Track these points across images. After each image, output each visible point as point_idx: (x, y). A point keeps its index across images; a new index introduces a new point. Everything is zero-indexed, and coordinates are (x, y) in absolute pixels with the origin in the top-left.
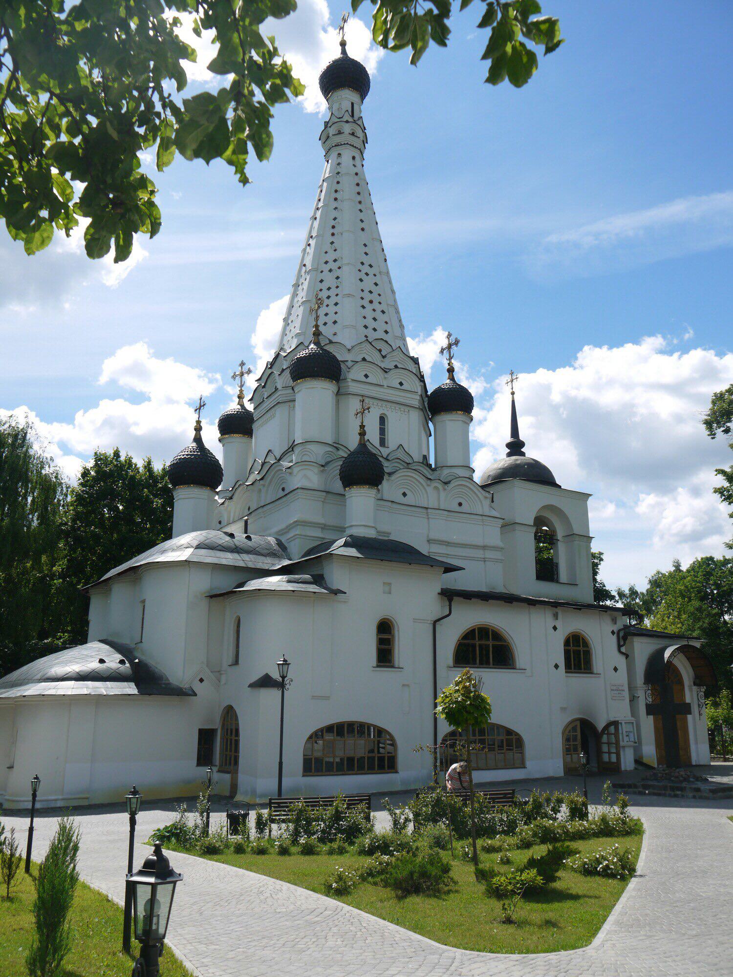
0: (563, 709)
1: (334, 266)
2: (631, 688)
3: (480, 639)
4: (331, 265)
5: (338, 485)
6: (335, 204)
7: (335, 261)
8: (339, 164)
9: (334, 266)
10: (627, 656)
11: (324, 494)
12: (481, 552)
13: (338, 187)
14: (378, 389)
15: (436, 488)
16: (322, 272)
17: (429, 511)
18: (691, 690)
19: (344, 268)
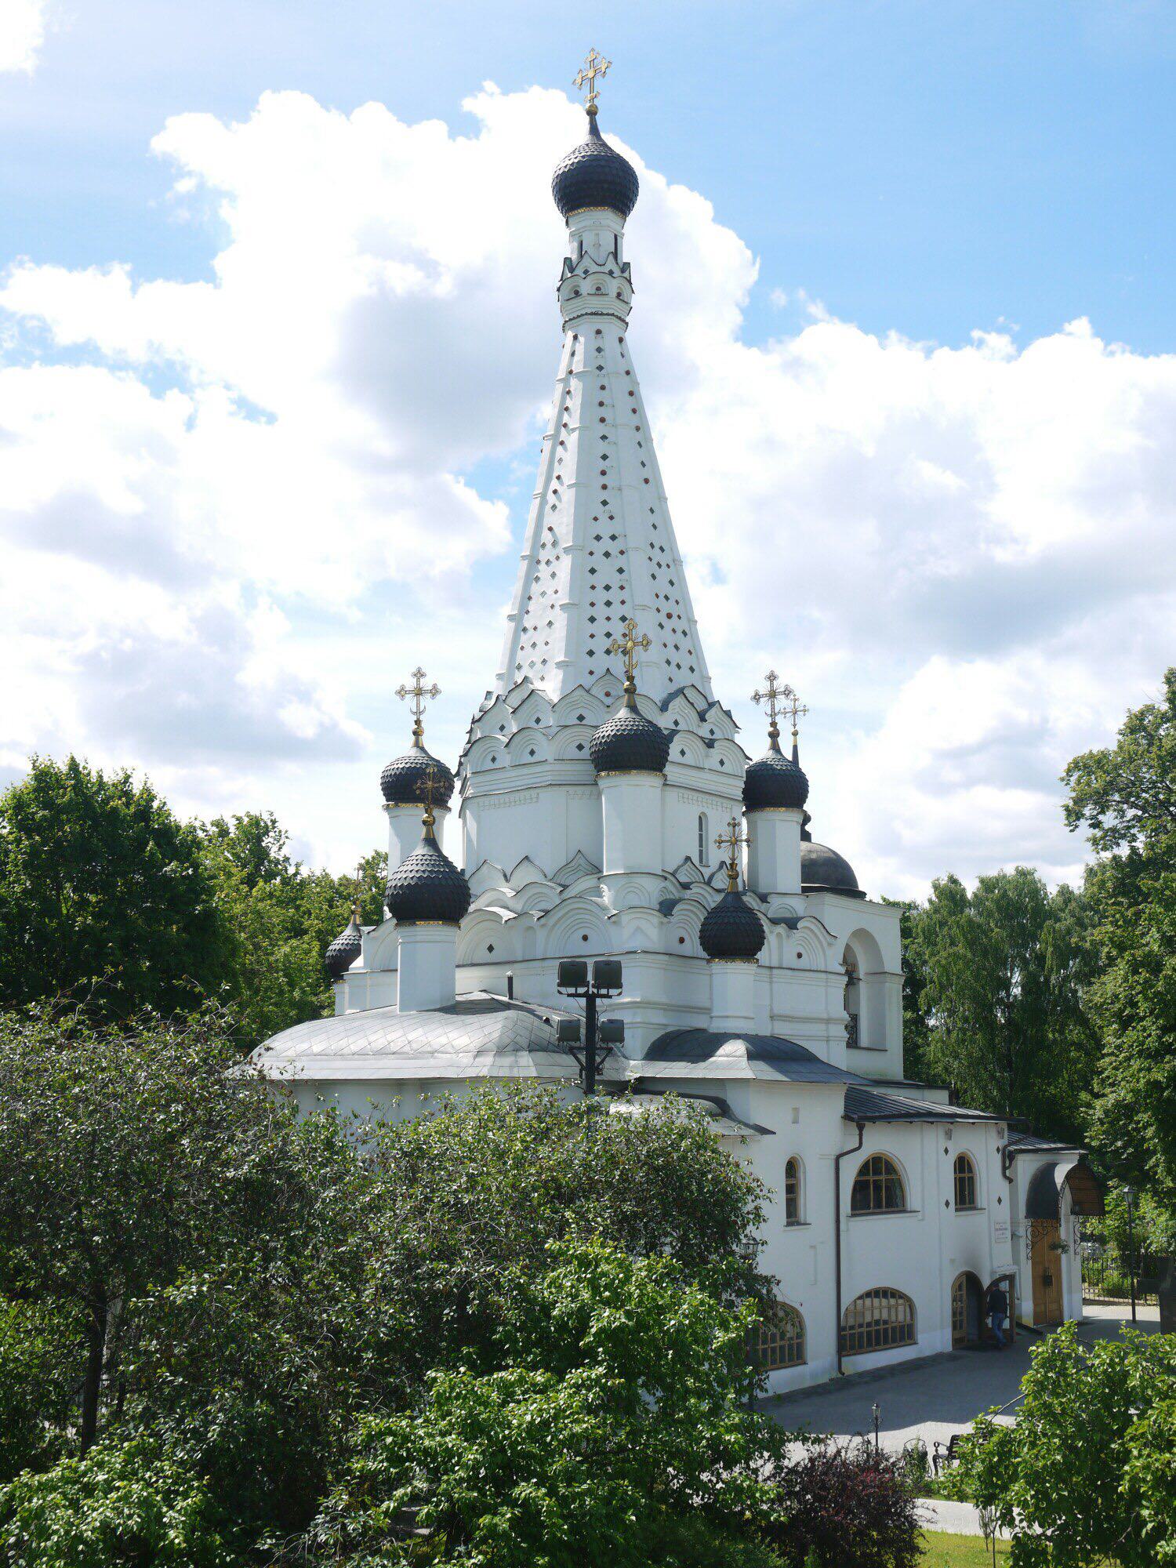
0: (952, 1261)
1: (613, 548)
2: (1014, 1222)
3: (875, 1173)
4: (606, 544)
5: (694, 946)
6: (602, 429)
7: (613, 538)
8: (599, 350)
9: (613, 548)
10: (1011, 1181)
11: (666, 958)
12: (823, 1027)
13: (604, 396)
14: (694, 773)
15: (779, 935)
16: (591, 554)
17: (775, 971)
18: (1067, 1222)
19: (631, 554)
